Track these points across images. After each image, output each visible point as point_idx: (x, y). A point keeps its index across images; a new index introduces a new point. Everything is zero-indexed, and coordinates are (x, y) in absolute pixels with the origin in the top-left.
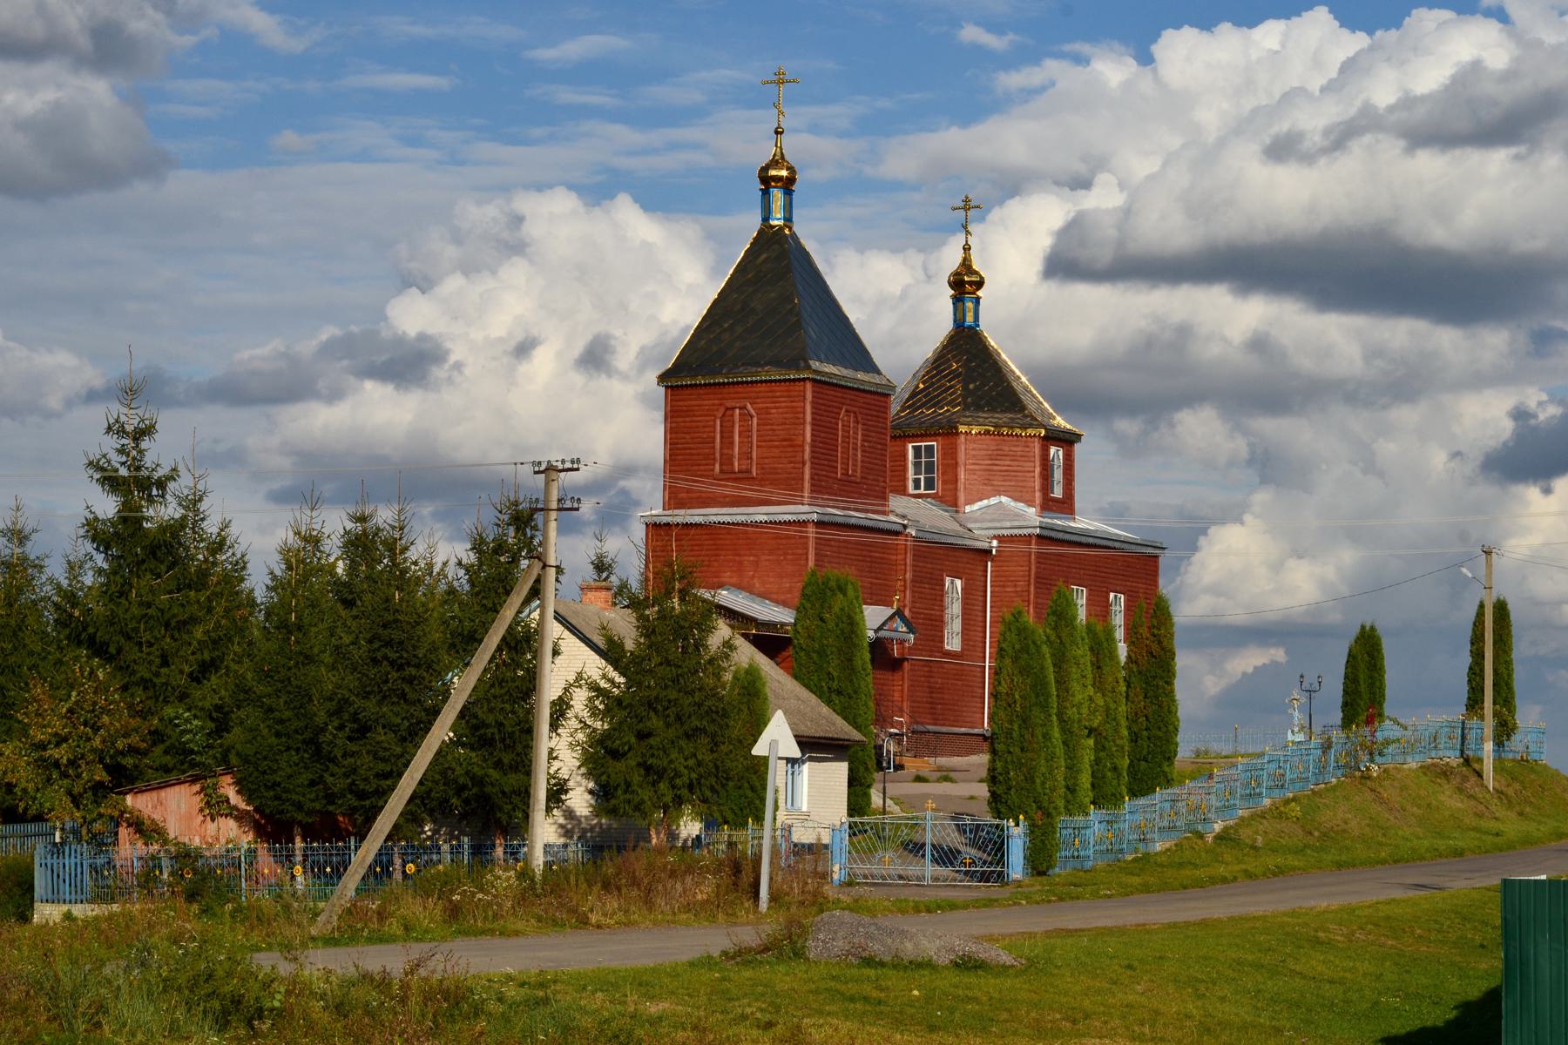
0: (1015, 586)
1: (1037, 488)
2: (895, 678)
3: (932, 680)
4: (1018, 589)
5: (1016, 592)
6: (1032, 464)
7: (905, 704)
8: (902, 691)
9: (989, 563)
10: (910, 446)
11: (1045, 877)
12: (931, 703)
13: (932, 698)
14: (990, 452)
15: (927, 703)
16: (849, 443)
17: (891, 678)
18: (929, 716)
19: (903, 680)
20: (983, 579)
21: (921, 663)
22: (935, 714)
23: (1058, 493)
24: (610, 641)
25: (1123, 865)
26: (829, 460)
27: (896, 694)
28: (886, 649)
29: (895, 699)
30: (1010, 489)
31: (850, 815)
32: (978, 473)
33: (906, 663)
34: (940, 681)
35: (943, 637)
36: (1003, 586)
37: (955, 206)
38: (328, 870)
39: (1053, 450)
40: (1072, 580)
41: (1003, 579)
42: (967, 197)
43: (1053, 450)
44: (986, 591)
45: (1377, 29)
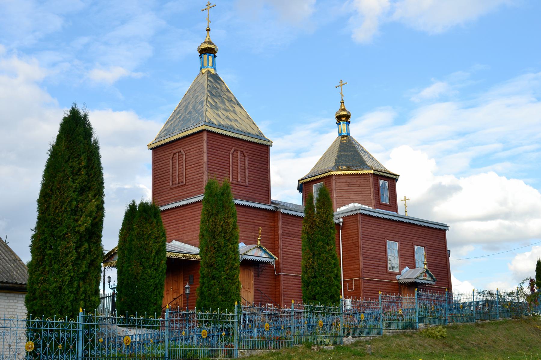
0: (352, 240)
1: (372, 198)
4: (354, 241)
5: (353, 242)
6: (369, 187)
9: (340, 231)
10: (313, 185)
11: (284, 273)
14: (348, 183)
16: (238, 166)
20: (337, 238)
23: (386, 200)
25: (348, 312)
30: (358, 199)
36: (347, 241)
37: (337, 86)
38: (60, 346)
39: (381, 182)
40: (388, 238)
41: (347, 237)
42: (341, 81)
43: (381, 182)
44: (339, 244)
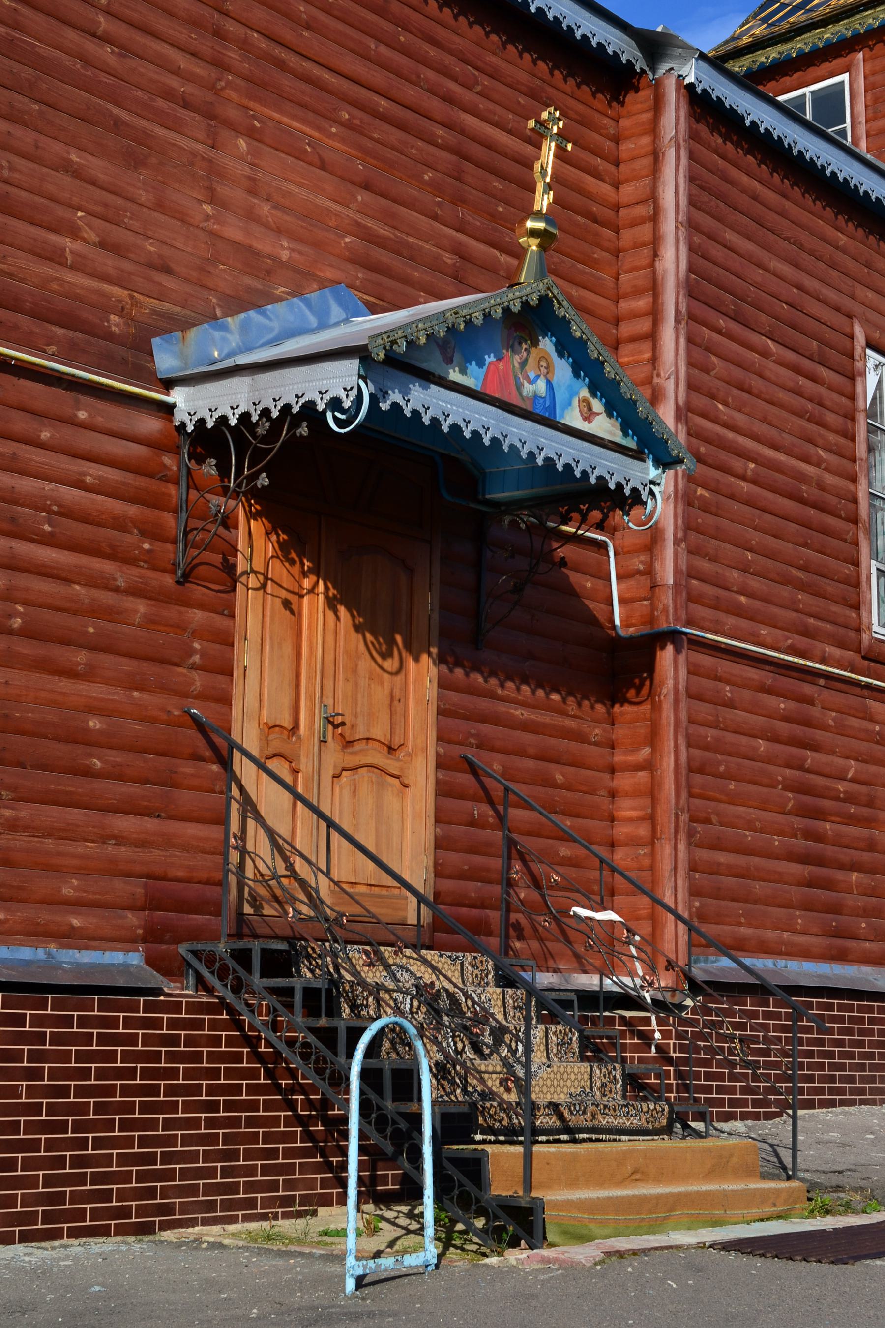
2: (620, 732)
3: (811, 757)
7: (665, 851)
8: (652, 792)
12: (804, 859)
13: (809, 835)
15: (792, 857)
17: (597, 732)
18: (800, 919)
19: (653, 738)
21: (753, 674)
22: (835, 909)
24: (278, 227)
26: (449, 99)
27: (627, 809)
28: (593, 621)
29: (621, 831)
31: (332, 1205)
32: (135, 225)
33: (666, 656)
34: (853, 768)
35: (856, 583)
45: (810, 52)
